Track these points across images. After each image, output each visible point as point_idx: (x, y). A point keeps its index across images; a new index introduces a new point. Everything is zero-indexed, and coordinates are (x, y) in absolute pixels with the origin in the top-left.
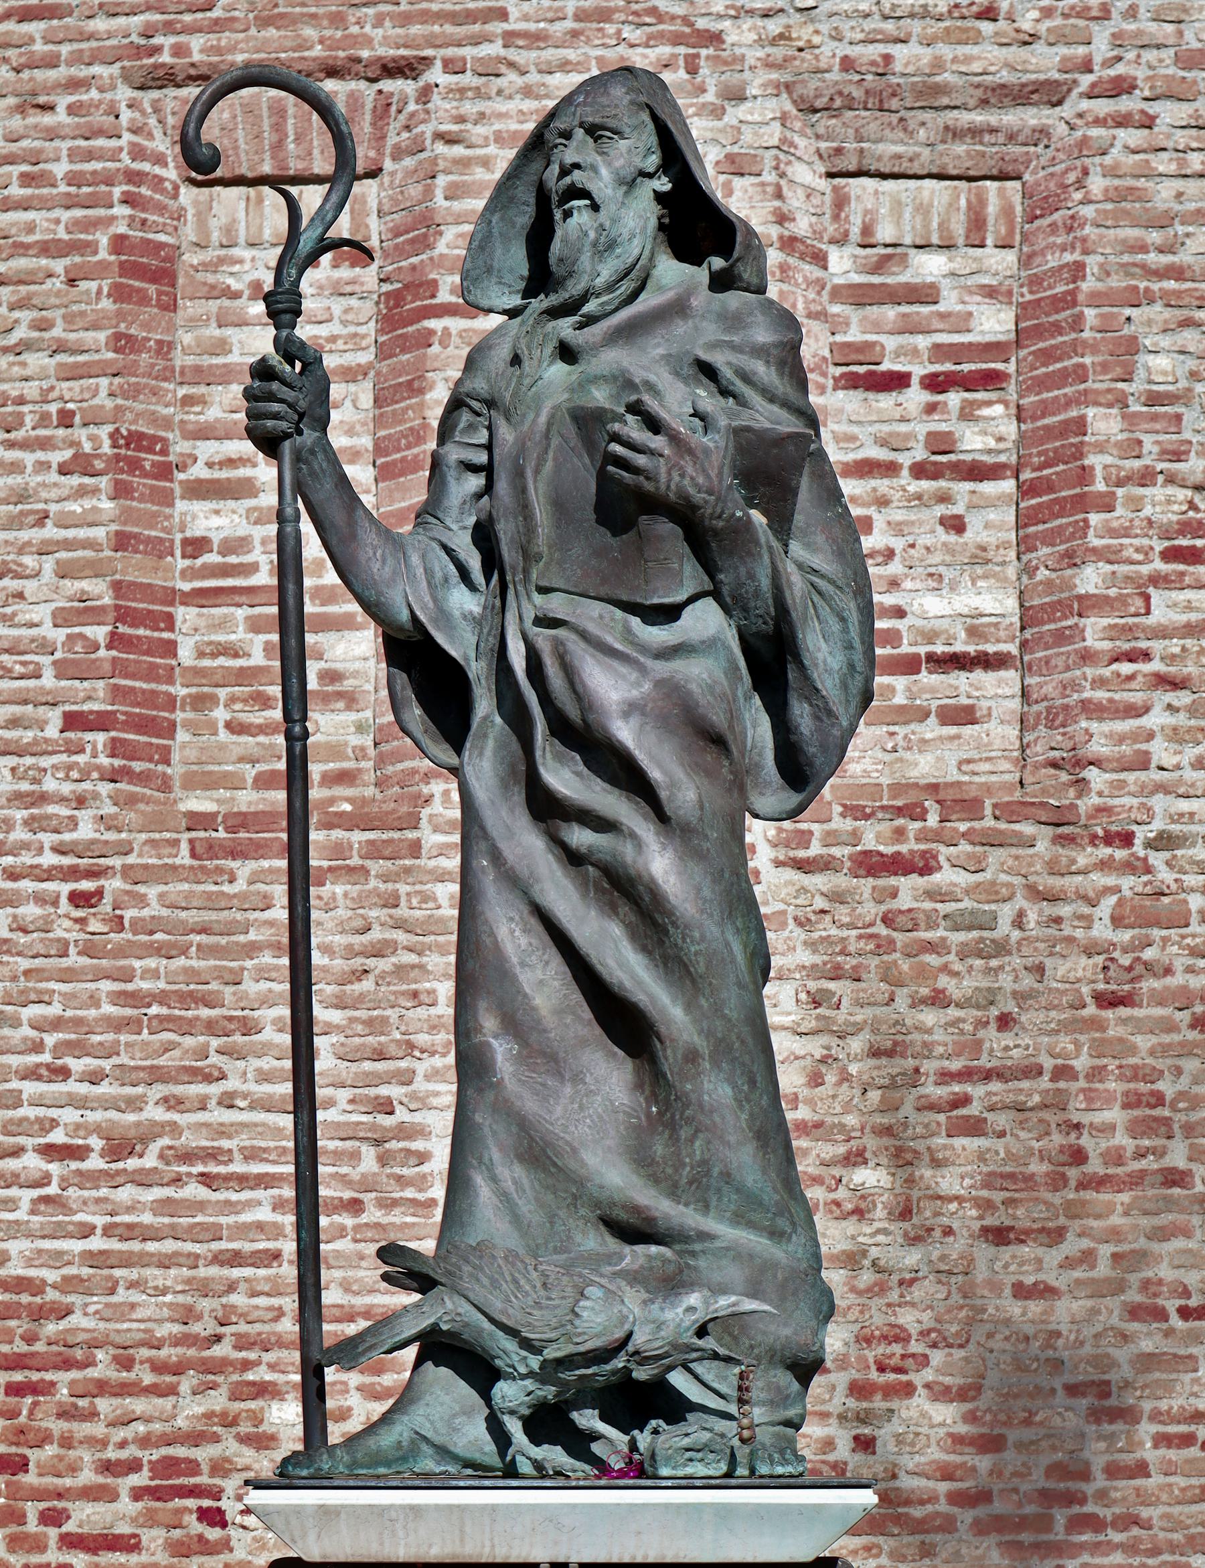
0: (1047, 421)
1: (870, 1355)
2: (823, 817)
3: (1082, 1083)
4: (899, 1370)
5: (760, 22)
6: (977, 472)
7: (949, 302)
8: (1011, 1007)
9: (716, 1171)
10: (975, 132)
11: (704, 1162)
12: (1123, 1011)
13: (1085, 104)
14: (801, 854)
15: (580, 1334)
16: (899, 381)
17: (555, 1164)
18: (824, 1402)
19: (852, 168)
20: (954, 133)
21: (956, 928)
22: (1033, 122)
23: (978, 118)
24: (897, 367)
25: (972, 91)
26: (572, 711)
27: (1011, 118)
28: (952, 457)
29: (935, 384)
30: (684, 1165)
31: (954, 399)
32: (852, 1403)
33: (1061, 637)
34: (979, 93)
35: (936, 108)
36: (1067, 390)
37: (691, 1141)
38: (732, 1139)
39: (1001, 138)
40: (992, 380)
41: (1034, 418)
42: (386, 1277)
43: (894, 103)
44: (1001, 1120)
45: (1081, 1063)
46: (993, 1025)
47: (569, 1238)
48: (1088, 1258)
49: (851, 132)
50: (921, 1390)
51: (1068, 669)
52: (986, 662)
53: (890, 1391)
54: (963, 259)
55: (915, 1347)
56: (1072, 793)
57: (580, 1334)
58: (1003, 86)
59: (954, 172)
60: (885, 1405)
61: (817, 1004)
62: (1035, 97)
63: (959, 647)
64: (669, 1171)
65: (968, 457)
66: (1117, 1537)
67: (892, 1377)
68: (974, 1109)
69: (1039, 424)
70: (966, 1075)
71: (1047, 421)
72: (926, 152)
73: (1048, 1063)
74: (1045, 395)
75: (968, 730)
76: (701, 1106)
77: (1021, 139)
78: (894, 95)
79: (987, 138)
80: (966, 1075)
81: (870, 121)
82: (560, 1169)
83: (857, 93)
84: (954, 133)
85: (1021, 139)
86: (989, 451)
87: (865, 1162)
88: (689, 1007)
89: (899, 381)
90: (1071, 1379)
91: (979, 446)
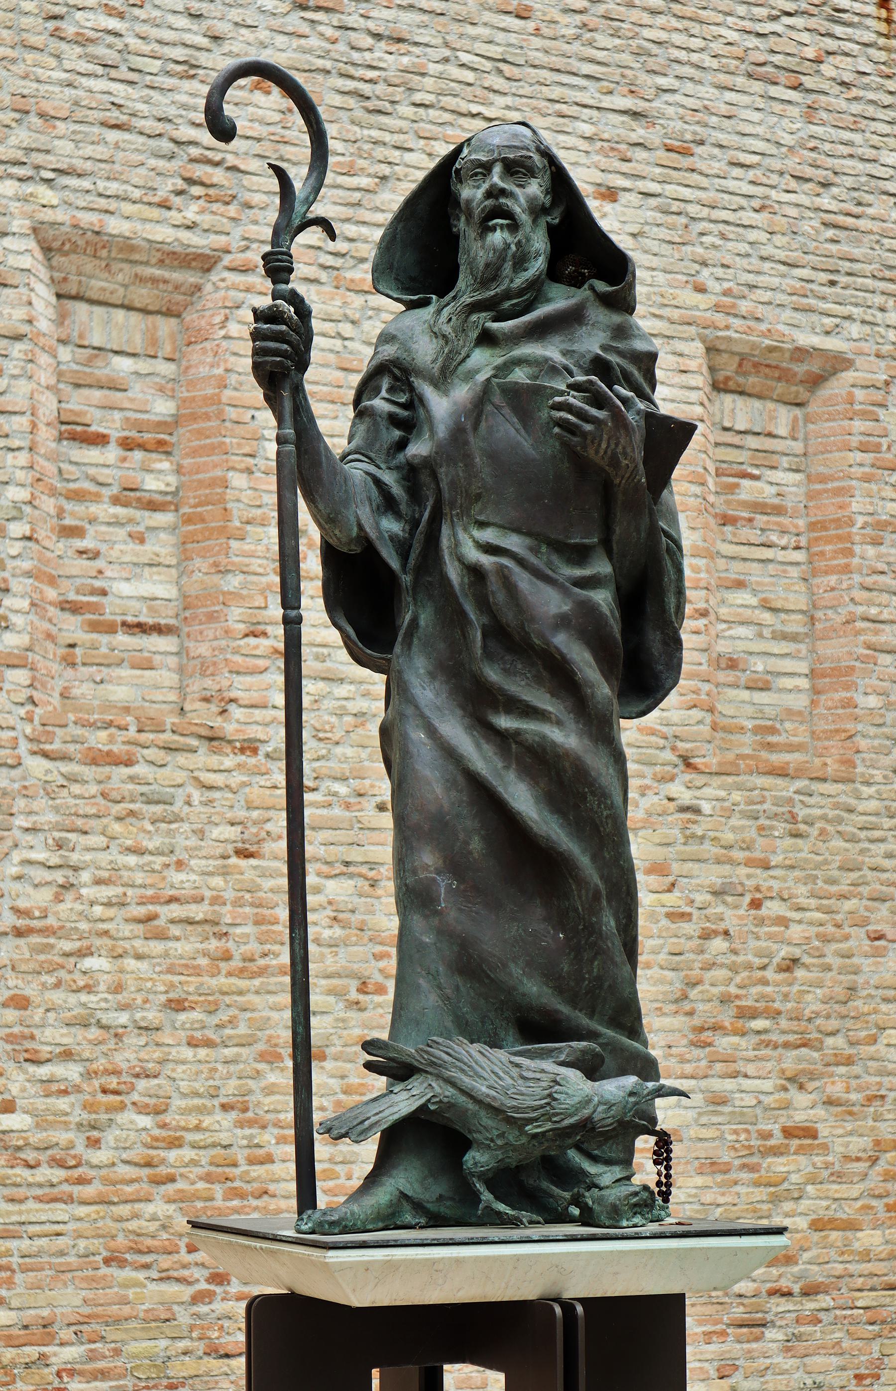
0: (201, 476)
1: (96, 1083)
2: (62, 722)
3: (229, 907)
4: (116, 1092)
5: (17, 184)
6: (153, 506)
7: (137, 391)
8: (184, 856)
9: (606, 984)
10: (154, 281)
11: (599, 979)
12: (252, 862)
13: (226, 274)
14: (47, 747)
15: (557, 1114)
16: (100, 440)
17: (488, 977)
18: (67, 1114)
19: (73, 292)
20: (140, 280)
21: (149, 802)
22: (192, 280)
23: (158, 272)
24: (102, 430)
25: (154, 253)
26: (509, 617)
27: (177, 276)
28: (138, 494)
29: (127, 445)
30: (584, 979)
31: (138, 455)
32: (85, 1116)
33: (212, 617)
34: (159, 255)
35: (131, 262)
36: (214, 458)
37: (592, 961)
38: (618, 959)
39: (170, 288)
40: (162, 448)
41: (190, 473)
42: (369, 1066)
43: (104, 253)
44: (175, 930)
45: (229, 895)
46: (173, 867)
47: (496, 1034)
48: (233, 1022)
49: (74, 268)
50: (130, 1106)
51: (216, 639)
52: (159, 629)
53: (110, 1109)
54: (143, 366)
55: (125, 1078)
56: (219, 719)
57: (557, 1114)
58: (174, 253)
59: (138, 305)
60: (107, 1117)
61: (60, 847)
62: (194, 264)
63: (142, 619)
64: (572, 984)
65: (147, 495)
66: (254, 1203)
67: (112, 1098)
68: (161, 922)
69: (195, 477)
70: (154, 900)
71: (201, 476)
72: (121, 291)
73: (208, 894)
74: (198, 460)
75: (147, 673)
76: (600, 934)
77: (183, 289)
78: (104, 247)
79: (161, 286)
80: (154, 900)
81: (89, 265)
82: (492, 980)
83: (81, 243)
84: (140, 280)
85: (183, 289)
86: (161, 492)
87: (92, 954)
88: (594, 858)
89: (100, 440)
90: (224, 1100)
91: (153, 488)
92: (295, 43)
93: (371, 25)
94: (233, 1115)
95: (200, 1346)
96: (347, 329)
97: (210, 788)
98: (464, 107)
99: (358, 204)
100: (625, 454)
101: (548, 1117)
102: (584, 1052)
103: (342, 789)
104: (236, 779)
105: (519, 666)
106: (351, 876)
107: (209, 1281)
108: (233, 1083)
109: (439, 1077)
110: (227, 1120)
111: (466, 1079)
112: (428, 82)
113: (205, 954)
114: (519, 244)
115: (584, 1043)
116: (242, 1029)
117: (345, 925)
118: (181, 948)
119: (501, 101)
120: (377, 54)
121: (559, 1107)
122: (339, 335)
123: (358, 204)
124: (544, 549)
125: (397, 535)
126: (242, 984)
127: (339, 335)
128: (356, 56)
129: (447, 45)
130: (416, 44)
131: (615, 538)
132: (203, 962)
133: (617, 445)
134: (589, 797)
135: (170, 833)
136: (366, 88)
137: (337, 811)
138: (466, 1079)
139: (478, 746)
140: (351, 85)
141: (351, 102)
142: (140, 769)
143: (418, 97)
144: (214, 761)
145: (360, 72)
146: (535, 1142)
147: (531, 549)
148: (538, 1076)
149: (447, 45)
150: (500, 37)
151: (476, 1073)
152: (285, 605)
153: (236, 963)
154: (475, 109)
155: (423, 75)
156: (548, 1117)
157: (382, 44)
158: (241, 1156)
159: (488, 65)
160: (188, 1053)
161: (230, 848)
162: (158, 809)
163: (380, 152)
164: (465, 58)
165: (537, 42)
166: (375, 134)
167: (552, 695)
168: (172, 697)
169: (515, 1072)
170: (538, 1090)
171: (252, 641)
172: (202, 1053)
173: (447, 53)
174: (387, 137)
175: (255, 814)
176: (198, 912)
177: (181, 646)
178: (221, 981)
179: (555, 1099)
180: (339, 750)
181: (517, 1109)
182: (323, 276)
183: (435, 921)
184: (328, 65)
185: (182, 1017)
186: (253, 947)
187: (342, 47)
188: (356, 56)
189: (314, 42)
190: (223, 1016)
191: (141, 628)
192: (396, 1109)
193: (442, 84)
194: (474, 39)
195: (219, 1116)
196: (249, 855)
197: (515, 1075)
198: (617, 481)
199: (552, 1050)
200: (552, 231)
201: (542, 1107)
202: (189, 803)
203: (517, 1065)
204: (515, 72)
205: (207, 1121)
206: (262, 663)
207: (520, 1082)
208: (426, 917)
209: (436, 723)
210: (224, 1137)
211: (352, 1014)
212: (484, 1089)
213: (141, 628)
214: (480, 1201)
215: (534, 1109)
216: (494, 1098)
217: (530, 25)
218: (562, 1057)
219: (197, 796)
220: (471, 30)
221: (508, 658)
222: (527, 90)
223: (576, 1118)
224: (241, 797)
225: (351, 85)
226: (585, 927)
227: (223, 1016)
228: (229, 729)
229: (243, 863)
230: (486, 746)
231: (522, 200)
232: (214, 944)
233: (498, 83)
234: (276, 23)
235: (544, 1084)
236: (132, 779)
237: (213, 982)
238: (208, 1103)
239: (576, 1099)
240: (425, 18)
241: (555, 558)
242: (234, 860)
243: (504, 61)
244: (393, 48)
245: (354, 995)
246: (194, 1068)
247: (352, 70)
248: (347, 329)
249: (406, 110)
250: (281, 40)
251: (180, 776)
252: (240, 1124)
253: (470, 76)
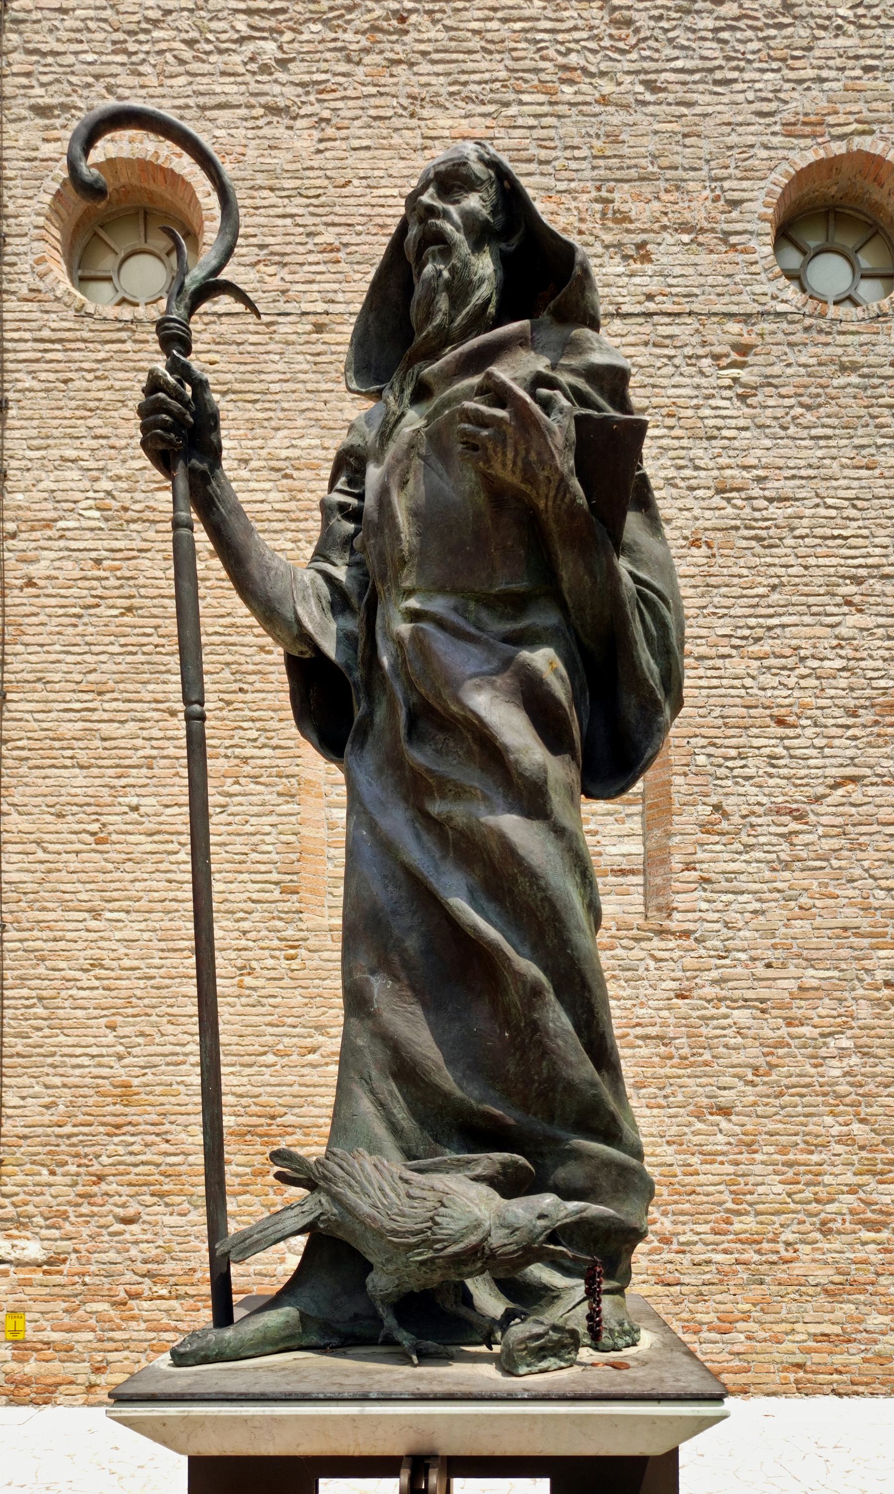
8: (644, 1000)
15: (439, 1241)
30: (533, 1081)
57: (439, 1241)
92: (717, 513)
93: (767, 493)
94: (675, 1147)
95: (653, 1279)
96: (748, 682)
97: (661, 960)
98: (829, 532)
99: (757, 605)
100: (542, 462)
101: (428, 1243)
102: (504, 1165)
103: (743, 956)
104: (676, 954)
105: (451, 744)
106: (749, 1007)
107: (660, 1241)
108: (675, 1129)
109: (328, 1192)
110: (671, 1149)
111: (349, 1193)
112: (805, 522)
113: (658, 1055)
114: (453, 270)
115: (506, 1155)
116: (680, 1098)
117: (744, 1037)
118: (644, 1051)
119: (855, 524)
120: (771, 510)
121: (441, 1233)
122: (744, 687)
123: (757, 605)
124: (472, 606)
125: (352, 632)
126: (681, 1072)
127: (744, 687)
128: (757, 515)
129: (817, 496)
130: (797, 500)
131: (565, 586)
132: (656, 1059)
133: (528, 451)
134: (520, 879)
135: (635, 988)
136: (763, 533)
137: (739, 970)
138: (349, 1193)
139: (418, 837)
140: (752, 533)
141: (753, 543)
142: (619, 952)
143: (797, 533)
144: (663, 945)
145: (760, 524)
146: (424, 1269)
147: (455, 609)
148: (425, 1194)
149: (817, 496)
150: (855, 484)
151: (363, 1188)
152: (187, 701)
153: (676, 1061)
154: (836, 532)
155: (801, 518)
156: (428, 1243)
157: (775, 504)
158: (678, 1170)
159: (846, 503)
160: (647, 1112)
161: (672, 994)
162: (629, 974)
163: (772, 571)
164: (830, 501)
165: (882, 482)
166: (769, 560)
167: (483, 770)
168: (642, 909)
169: (402, 1187)
170: (421, 1211)
171: (686, 873)
172: (655, 1111)
173: (818, 500)
174: (777, 561)
175: (688, 974)
176: (653, 1031)
177: (645, 880)
178: (668, 1071)
179: (436, 1224)
180: (741, 933)
181: (395, 1233)
182: (734, 652)
183: (369, 1023)
184: (738, 523)
185: (643, 1091)
186: (686, 1051)
187: (748, 510)
188: (757, 515)
189: (730, 510)
190: (668, 1091)
191: (623, 873)
192: (279, 1227)
193: (814, 521)
194: (836, 488)
195: (666, 1147)
196: (684, 997)
197: (402, 1193)
198: (542, 504)
199: (469, 1162)
200: (504, 261)
201: (422, 1232)
202: (647, 969)
203: (406, 1181)
204: (865, 504)
205: (658, 1150)
206: (693, 886)
207: (406, 1200)
208: (362, 1019)
209: (378, 818)
210: (669, 1160)
211: (749, 1088)
212: (367, 1209)
213: (623, 873)
214: (382, 1326)
215: (415, 1233)
216: (374, 1219)
217: (877, 472)
218: (479, 1171)
219: (652, 964)
220: (834, 483)
221: (440, 737)
222: (873, 514)
223: (462, 1245)
224: (679, 964)
225: (752, 533)
226: (527, 1024)
227: (668, 1091)
228: (673, 925)
229: (680, 1002)
230: (425, 837)
231: (456, 217)
232: (663, 1049)
233: (853, 513)
234: (704, 504)
235: (428, 1204)
236: (613, 957)
237: (662, 1071)
238: (659, 1140)
239: (462, 1224)
240: (803, 482)
241: (484, 615)
242: (675, 1001)
243: (858, 498)
244: (781, 505)
245: (750, 1077)
246: (651, 1120)
247: (754, 524)
248: (748, 682)
249: (789, 542)
250: (708, 514)
251: (643, 954)
252: (679, 1153)
253: (833, 512)
